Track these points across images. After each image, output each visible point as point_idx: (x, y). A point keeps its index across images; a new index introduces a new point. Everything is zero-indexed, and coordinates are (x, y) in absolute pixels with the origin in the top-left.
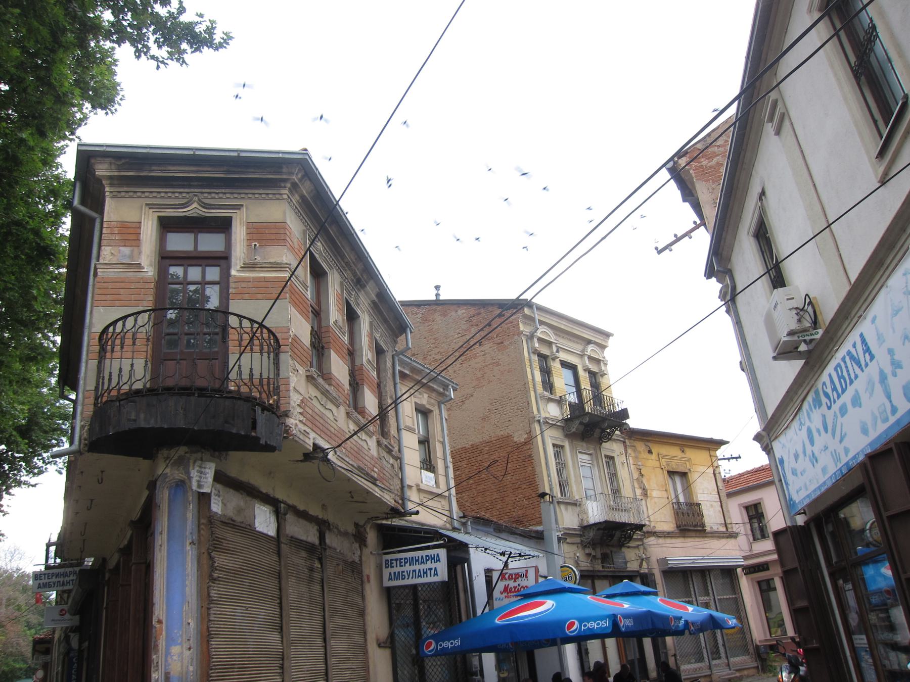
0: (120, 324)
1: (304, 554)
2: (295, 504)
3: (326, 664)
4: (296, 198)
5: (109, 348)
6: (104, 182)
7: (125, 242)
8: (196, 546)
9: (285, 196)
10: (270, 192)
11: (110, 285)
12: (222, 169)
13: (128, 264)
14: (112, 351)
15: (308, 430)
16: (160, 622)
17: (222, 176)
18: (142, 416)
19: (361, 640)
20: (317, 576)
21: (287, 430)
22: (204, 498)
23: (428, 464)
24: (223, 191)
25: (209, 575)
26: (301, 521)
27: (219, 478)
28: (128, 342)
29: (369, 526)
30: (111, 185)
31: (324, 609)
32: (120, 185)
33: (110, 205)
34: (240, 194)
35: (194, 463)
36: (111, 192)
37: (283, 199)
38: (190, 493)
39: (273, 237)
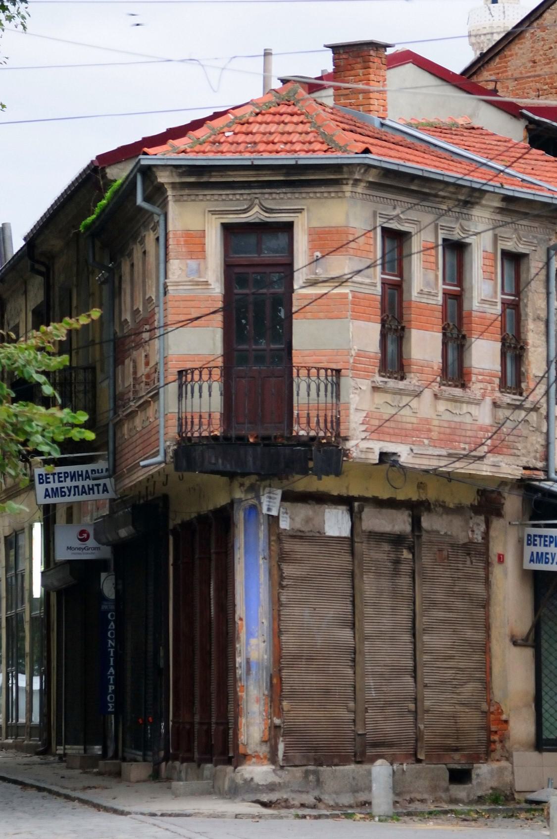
1: (386, 547)
2: (376, 495)
3: (415, 660)
7: (191, 255)
16: (241, 619)
18: (220, 461)
19: (479, 636)
20: (405, 568)
21: (346, 453)
22: (273, 521)
24: (284, 190)
25: (278, 582)
26: (384, 511)
31: (414, 603)
33: (173, 208)
35: (264, 489)
38: (261, 517)
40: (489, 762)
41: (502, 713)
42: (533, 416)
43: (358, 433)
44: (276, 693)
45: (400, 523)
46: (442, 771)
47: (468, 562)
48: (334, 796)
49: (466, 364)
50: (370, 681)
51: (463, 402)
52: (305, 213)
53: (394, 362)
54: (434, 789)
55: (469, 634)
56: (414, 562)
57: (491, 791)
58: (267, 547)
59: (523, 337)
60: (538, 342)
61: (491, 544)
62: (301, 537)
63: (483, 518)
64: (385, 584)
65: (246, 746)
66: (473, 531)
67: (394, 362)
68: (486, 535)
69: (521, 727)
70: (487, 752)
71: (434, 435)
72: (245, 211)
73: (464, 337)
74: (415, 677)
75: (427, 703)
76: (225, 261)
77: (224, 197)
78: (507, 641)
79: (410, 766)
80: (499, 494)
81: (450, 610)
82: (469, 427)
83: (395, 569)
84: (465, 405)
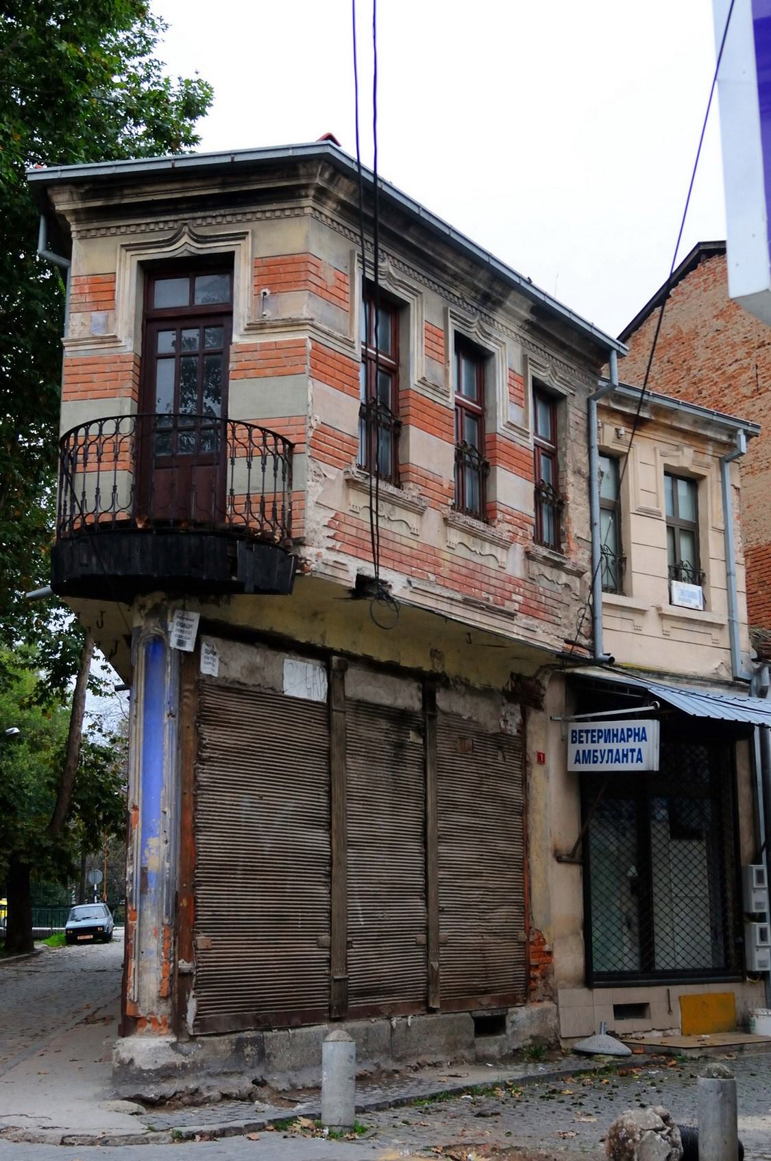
0: (95, 426)
1: (384, 724)
3: (426, 877)
4: (328, 209)
5: (80, 457)
8: (176, 719)
9: (308, 210)
11: (81, 370)
12: (215, 182)
15: (341, 558)
16: (135, 808)
17: (216, 191)
18: (94, 559)
19: (515, 849)
21: (300, 563)
22: (189, 661)
23: (687, 569)
24: (222, 212)
26: (381, 677)
27: (207, 628)
28: (108, 447)
29: (547, 678)
30: (78, 221)
31: (426, 802)
32: (89, 220)
33: (77, 247)
34: (245, 214)
37: (305, 215)
39: (289, 277)
40: (529, 1004)
41: (544, 943)
42: (576, 583)
43: (321, 538)
44: (183, 924)
45: (407, 697)
46: (464, 1019)
47: (500, 758)
48: (291, 1074)
49: (490, 499)
50: (357, 904)
51: (485, 540)
52: (249, 238)
53: (382, 463)
54: (453, 1046)
55: (502, 846)
56: (425, 748)
57: (530, 1042)
58: (177, 698)
60: (579, 500)
61: (529, 740)
62: (239, 692)
63: (518, 707)
64: (382, 772)
65: (136, 1004)
66: (506, 721)
67: (382, 463)
68: (523, 727)
69: (568, 959)
70: (526, 995)
71: (444, 571)
72: (170, 242)
73: (486, 465)
74: (426, 899)
75: (444, 934)
76: (144, 314)
77: (143, 228)
78: (550, 855)
79: (417, 1019)
80: (539, 683)
81: (475, 814)
82: (493, 574)
83: (396, 755)
84: (487, 545)
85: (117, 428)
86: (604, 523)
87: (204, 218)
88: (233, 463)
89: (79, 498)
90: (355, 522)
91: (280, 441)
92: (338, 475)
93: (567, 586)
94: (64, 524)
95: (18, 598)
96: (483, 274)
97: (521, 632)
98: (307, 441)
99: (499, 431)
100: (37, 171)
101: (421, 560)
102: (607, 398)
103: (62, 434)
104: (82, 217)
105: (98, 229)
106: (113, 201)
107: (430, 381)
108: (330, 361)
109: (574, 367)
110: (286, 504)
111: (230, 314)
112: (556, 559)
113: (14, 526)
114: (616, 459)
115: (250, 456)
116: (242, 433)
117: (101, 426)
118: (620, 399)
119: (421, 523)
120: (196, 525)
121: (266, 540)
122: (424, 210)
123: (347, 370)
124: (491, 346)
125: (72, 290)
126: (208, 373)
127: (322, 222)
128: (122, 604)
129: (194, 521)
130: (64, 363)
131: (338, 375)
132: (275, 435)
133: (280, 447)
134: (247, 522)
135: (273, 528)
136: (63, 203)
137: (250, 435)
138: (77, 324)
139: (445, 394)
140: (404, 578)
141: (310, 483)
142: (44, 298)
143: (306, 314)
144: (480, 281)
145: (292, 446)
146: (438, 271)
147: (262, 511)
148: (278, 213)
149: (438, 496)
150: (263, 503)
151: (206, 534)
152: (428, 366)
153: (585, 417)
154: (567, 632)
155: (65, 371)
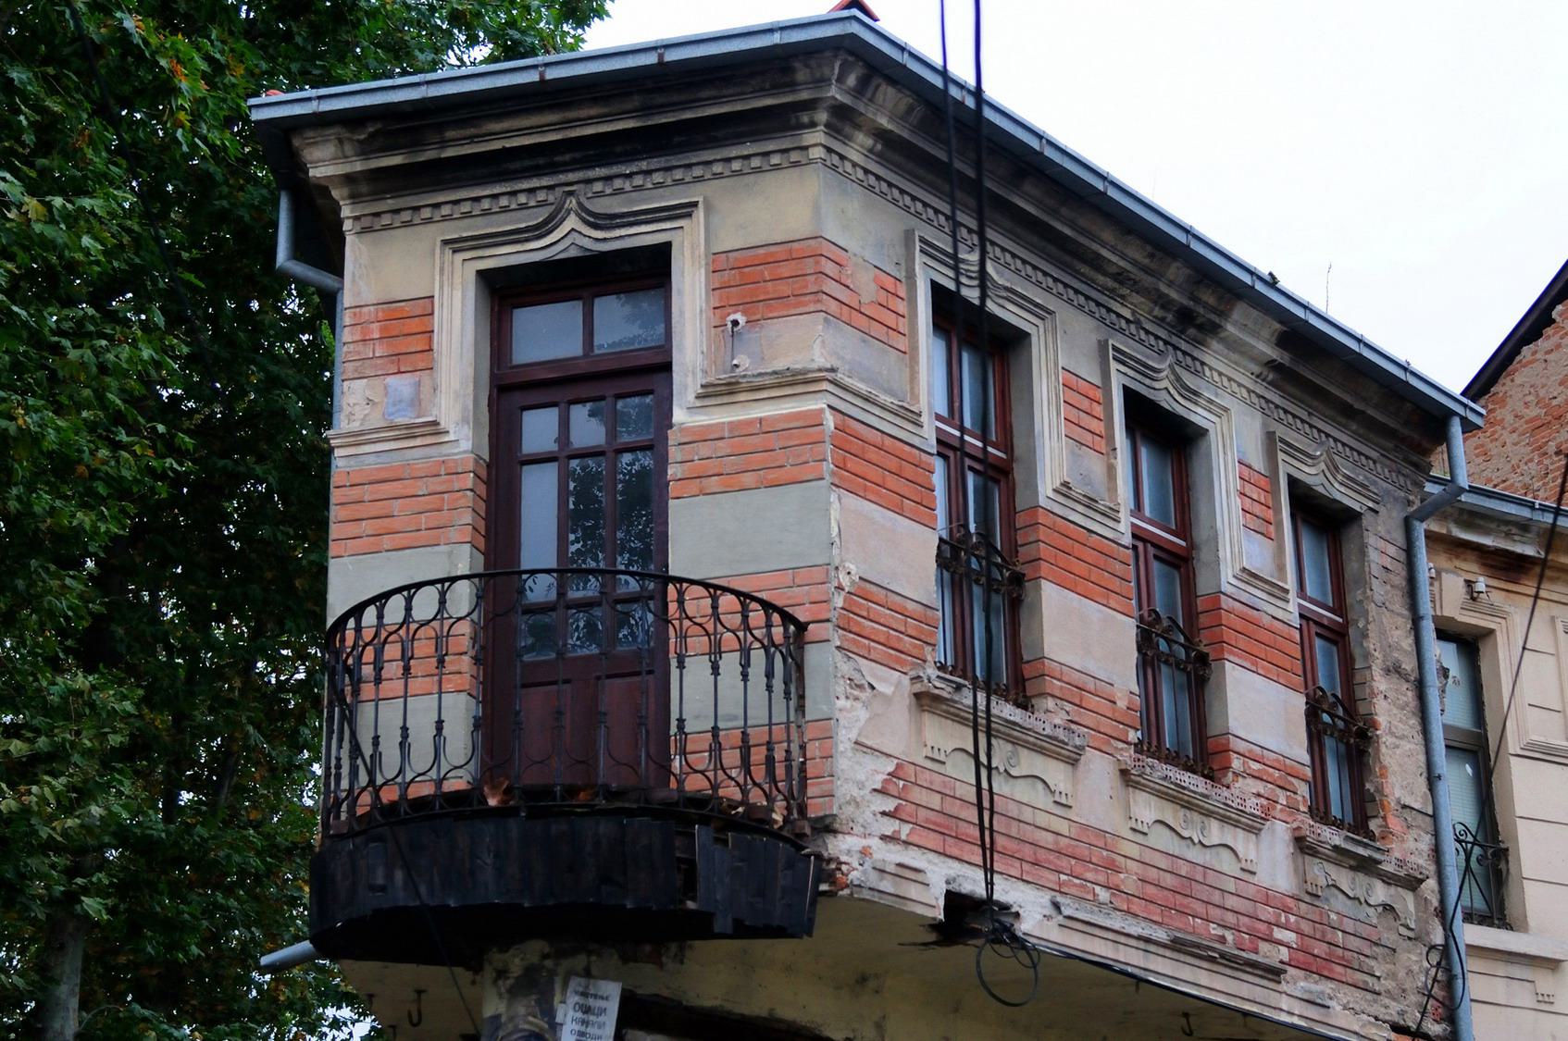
0: (397, 603)
4: (858, 148)
5: (367, 671)
6: (335, 194)
9: (817, 153)
10: (771, 146)
11: (367, 492)
13: (408, 427)
14: (378, 680)
15: (913, 858)
18: (399, 876)
21: (827, 870)
24: (644, 165)
28: (423, 647)
30: (355, 198)
32: (377, 195)
33: (355, 251)
34: (689, 166)
36: (356, 218)
37: (811, 162)
39: (784, 288)
42: (1407, 902)
43: (868, 815)
49: (1214, 729)
51: (1209, 814)
52: (700, 214)
53: (989, 659)
59: (1362, 709)
60: (1401, 728)
67: (989, 659)
71: (1130, 884)
73: (1203, 660)
76: (493, 376)
77: (486, 204)
82: (1230, 885)
84: (1214, 825)
85: (442, 602)
86: (1457, 778)
87: (608, 179)
88: (681, 666)
89: (367, 750)
90: (938, 782)
91: (776, 618)
92: (898, 685)
93: (1388, 908)
94: (338, 803)
95: (259, 987)
96: (1176, 271)
97: (1298, 1008)
98: (833, 615)
99: (1225, 588)
100: (273, 105)
101: (1078, 860)
102: (1444, 518)
103: (330, 621)
104: (364, 189)
105: (397, 211)
106: (427, 154)
107: (1079, 490)
108: (872, 454)
109: (1374, 454)
110: (795, 748)
111: (667, 367)
112: (1361, 851)
113: (245, 839)
114: (1470, 643)
115: (716, 652)
116: (698, 603)
117: (409, 600)
118: (1473, 518)
119: (1075, 782)
120: (612, 795)
121: (755, 823)
122: (1050, 143)
123: (909, 471)
124: (1198, 416)
125: (346, 335)
126: (622, 508)
127: (846, 175)
128: (459, 970)
129: (606, 787)
130: (334, 481)
131: (892, 481)
132: (767, 606)
133: (778, 632)
134: (715, 787)
135: (768, 797)
136: (325, 163)
137: (715, 607)
138: (358, 402)
139: (1111, 515)
140: (1045, 898)
141: (842, 703)
142: (302, 386)
143: (821, 361)
144: (1171, 284)
145: (802, 627)
146: (1085, 269)
147: (746, 764)
148: (756, 162)
149: (1107, 726)
150: (745, 748)
151: (630, 813)
152: (1071, 458)
153: (1402, 557)
154: (1395, 1007)
155: (335, 496)
